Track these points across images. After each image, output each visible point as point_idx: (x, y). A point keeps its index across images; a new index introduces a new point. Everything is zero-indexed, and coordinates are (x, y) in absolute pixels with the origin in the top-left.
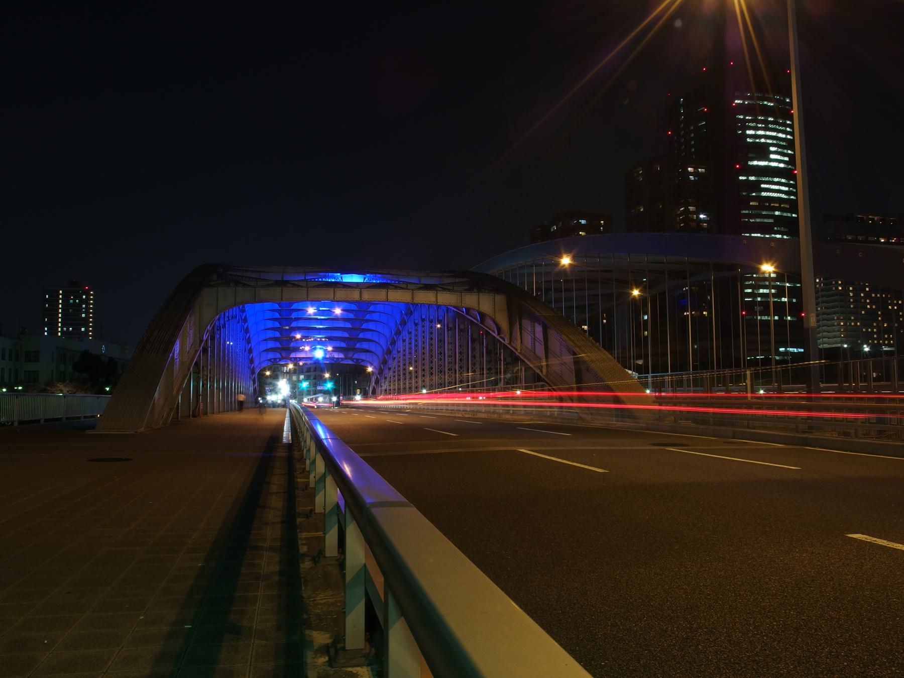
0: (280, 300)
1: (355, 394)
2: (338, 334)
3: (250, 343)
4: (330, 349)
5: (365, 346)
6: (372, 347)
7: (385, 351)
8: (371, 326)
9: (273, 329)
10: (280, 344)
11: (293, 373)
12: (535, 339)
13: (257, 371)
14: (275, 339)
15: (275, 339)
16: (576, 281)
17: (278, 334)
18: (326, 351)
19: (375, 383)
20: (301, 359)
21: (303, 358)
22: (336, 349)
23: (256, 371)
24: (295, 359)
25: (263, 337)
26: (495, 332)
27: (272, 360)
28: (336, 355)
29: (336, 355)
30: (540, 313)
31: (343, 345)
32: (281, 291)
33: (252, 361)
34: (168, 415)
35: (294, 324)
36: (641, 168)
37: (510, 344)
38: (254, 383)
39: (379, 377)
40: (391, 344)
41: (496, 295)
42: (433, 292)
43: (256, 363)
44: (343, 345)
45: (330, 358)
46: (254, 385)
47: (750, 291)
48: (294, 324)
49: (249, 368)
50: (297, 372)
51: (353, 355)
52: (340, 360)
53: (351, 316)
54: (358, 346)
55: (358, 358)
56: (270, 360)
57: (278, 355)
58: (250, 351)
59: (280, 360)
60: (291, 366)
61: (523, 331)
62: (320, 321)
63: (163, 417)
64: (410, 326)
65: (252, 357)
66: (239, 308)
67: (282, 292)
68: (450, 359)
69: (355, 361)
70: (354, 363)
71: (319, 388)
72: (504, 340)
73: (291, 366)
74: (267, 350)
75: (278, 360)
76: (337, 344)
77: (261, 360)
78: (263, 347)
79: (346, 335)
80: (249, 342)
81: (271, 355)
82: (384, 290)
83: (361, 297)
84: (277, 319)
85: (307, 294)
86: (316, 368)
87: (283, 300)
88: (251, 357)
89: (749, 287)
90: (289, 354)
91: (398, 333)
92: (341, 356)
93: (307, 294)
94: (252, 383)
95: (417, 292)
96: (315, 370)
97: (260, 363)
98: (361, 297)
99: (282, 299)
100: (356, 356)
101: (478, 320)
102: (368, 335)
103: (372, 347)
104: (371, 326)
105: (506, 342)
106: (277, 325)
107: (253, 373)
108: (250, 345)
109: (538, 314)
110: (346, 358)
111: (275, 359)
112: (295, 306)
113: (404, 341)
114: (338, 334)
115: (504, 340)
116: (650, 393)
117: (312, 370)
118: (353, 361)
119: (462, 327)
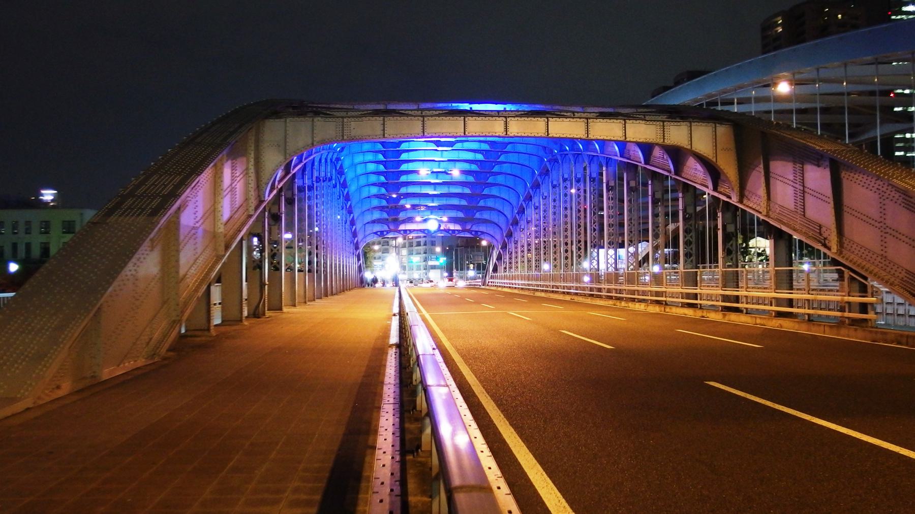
0: (382, 136)
1: (468, 269)
2: (455, 201)
3: (352, 213)
4: (445, 219)
5: (486, 215)
6: (494, 217)
7: (511, 221)
8: (494, 191)
9: (378, 196)
10: (388, 214)
11: (402, 247)
12: (804, 192)
13: (362, 246)
14: (381, 209)
15: (381, 209)
16: (825, 110)
17: (384, 203)
18: (441, 222)
19: (497, 259)
20: (411, 231)
21: (414, 230)
22: (452, 220)
23: (360, 247)
24: (405, 231)
25: (366, 206)
26: (707, 187)
27: (379, 233)
28: (452, 227)
29: (452, 227)
30: (821, 147)
31: (460, 215)
32: (382, 122)
33: (355, 234)
34: (164, 337)
35: (403, 190)
36: (780, 18)
37: (741, 202)
38: (359, 260)
39: (502, 252)
40: (518, 213)
41: (717, 125)
42: (619, 121)
43: (360, 237)
44: (460, 215)
45: (445, 230)
46: (358, 262)
47: (902, 153)
48: (403, 190)
49: (352, 242)
50: (407, 246)
51: (471, 227)
52: (456, 232)
53: (471, 179)
54: (478, 215)
55: (477, 230)
56: (376, 233)
57: (385, 228)
58: (353, 223)
59: (387, 233)
60: (400, 240)
61: (772, 181)
62: (433, 186)
63: (148, 343)
64: (545, 189)
65: (355, 229)
66: (336, 169)
67: (384, 124)
68: (611, 229)
69: (473, 233)
70: (472, 236)
71: (430, 263)
72: (730, 197)
73: (400, 240)
74: (374, 222)
75: (385, 233)
76: (453, 214)
77: (367, 233)
78: (368, 218)
79: (464, 203)
80: (350, 212)
81: (378, 228)
82: (543, 119)
83: (506, 130)
84: (383, 183)
85: (423, 127)
86: (426, 242)
87: (386, 135)
88: (353, 229)
89: (900, 149)
90: (398, 226)
91: (529, 198)
92: (458, 227)
93: (423, 127)
94: (356, 259)
95: (593, 122)
96: (425, 245)
97: (365, 237)
98: (506, 130)
99: (384, 135)
100: (475, 228)
101: (670, 172)
102: (490, 203)
103: (494, 217)
104: (494, 191)
105: (734, 200)
106: (383, 191)
107: (357, 248)
108: (352, 215)
109: (818, 148)
110: (464, 231)
111: (382, 232)
112: (404, 146)
113: (537, 208)
114: (455, 201)
115: (730, 197)
116: (438, 246)
117: (422, 244)
118: (471, 234)
119: (633, 184)
